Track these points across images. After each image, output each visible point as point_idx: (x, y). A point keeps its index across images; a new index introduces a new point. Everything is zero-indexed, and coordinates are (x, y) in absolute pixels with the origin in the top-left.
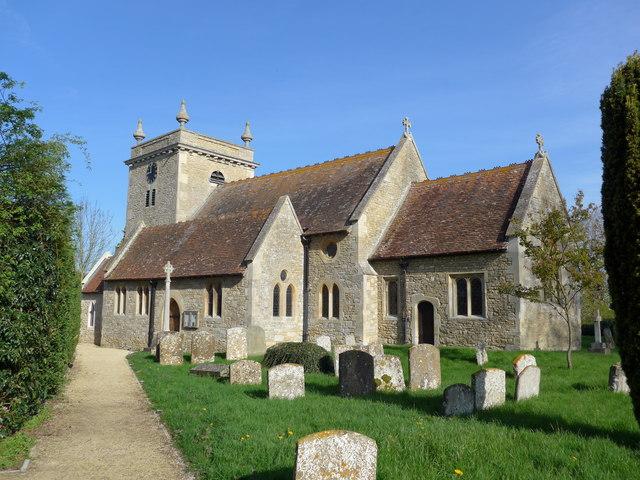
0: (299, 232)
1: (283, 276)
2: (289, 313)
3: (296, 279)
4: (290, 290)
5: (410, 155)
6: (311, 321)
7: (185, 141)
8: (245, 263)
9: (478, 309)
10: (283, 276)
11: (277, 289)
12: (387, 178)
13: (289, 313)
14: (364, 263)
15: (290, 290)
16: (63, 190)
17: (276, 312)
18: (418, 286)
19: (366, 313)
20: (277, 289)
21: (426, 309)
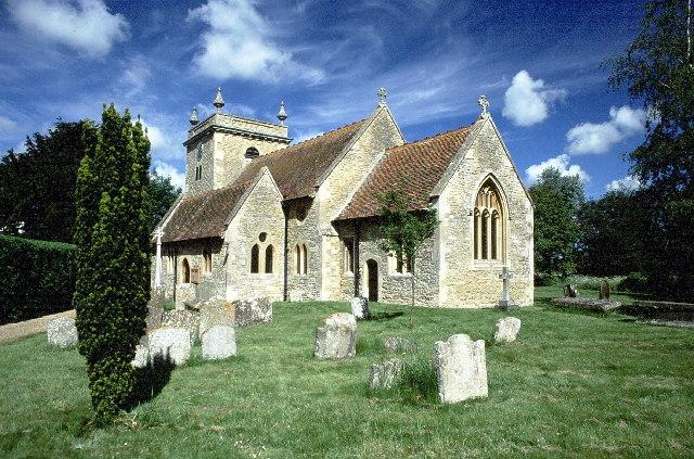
0: (281, 199)
1: (263, 237)
2: (494, 257)
3: (276, 240)
4: (270, 251)
5: (385, 123)
6: (289, 277)
7: (221, 124)
8: (435, 199)
9: (410, 269)
10: (263, 237)
11: (255, 250)
12: (356, 146)
13: (269, 269)
14: (325, 225)
15: (270, 251)
16: (556, 41)
17: (255, 269)
18: (368, 249)
19: (325, 271)
20: (255, 250)
21: (373, 265)
